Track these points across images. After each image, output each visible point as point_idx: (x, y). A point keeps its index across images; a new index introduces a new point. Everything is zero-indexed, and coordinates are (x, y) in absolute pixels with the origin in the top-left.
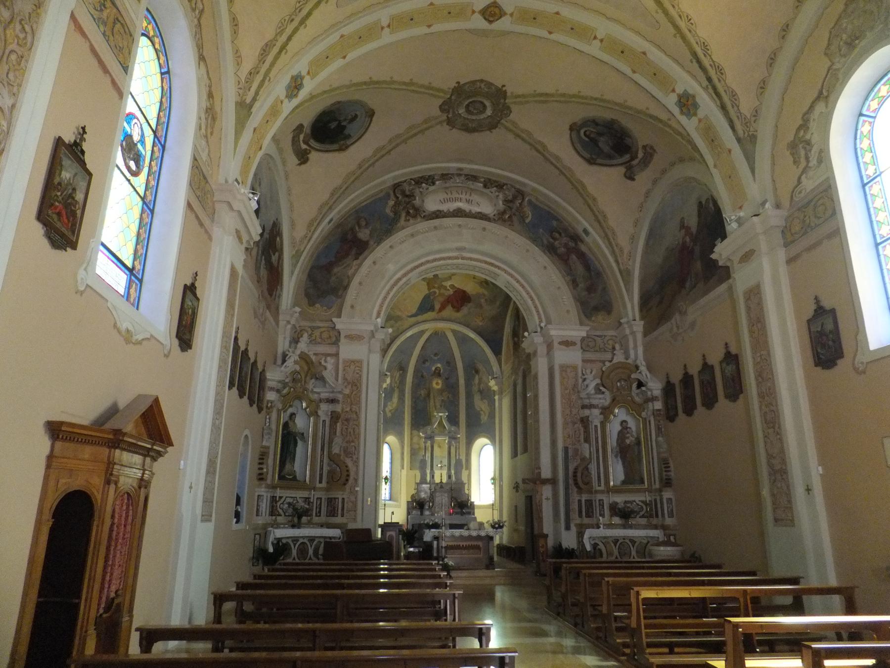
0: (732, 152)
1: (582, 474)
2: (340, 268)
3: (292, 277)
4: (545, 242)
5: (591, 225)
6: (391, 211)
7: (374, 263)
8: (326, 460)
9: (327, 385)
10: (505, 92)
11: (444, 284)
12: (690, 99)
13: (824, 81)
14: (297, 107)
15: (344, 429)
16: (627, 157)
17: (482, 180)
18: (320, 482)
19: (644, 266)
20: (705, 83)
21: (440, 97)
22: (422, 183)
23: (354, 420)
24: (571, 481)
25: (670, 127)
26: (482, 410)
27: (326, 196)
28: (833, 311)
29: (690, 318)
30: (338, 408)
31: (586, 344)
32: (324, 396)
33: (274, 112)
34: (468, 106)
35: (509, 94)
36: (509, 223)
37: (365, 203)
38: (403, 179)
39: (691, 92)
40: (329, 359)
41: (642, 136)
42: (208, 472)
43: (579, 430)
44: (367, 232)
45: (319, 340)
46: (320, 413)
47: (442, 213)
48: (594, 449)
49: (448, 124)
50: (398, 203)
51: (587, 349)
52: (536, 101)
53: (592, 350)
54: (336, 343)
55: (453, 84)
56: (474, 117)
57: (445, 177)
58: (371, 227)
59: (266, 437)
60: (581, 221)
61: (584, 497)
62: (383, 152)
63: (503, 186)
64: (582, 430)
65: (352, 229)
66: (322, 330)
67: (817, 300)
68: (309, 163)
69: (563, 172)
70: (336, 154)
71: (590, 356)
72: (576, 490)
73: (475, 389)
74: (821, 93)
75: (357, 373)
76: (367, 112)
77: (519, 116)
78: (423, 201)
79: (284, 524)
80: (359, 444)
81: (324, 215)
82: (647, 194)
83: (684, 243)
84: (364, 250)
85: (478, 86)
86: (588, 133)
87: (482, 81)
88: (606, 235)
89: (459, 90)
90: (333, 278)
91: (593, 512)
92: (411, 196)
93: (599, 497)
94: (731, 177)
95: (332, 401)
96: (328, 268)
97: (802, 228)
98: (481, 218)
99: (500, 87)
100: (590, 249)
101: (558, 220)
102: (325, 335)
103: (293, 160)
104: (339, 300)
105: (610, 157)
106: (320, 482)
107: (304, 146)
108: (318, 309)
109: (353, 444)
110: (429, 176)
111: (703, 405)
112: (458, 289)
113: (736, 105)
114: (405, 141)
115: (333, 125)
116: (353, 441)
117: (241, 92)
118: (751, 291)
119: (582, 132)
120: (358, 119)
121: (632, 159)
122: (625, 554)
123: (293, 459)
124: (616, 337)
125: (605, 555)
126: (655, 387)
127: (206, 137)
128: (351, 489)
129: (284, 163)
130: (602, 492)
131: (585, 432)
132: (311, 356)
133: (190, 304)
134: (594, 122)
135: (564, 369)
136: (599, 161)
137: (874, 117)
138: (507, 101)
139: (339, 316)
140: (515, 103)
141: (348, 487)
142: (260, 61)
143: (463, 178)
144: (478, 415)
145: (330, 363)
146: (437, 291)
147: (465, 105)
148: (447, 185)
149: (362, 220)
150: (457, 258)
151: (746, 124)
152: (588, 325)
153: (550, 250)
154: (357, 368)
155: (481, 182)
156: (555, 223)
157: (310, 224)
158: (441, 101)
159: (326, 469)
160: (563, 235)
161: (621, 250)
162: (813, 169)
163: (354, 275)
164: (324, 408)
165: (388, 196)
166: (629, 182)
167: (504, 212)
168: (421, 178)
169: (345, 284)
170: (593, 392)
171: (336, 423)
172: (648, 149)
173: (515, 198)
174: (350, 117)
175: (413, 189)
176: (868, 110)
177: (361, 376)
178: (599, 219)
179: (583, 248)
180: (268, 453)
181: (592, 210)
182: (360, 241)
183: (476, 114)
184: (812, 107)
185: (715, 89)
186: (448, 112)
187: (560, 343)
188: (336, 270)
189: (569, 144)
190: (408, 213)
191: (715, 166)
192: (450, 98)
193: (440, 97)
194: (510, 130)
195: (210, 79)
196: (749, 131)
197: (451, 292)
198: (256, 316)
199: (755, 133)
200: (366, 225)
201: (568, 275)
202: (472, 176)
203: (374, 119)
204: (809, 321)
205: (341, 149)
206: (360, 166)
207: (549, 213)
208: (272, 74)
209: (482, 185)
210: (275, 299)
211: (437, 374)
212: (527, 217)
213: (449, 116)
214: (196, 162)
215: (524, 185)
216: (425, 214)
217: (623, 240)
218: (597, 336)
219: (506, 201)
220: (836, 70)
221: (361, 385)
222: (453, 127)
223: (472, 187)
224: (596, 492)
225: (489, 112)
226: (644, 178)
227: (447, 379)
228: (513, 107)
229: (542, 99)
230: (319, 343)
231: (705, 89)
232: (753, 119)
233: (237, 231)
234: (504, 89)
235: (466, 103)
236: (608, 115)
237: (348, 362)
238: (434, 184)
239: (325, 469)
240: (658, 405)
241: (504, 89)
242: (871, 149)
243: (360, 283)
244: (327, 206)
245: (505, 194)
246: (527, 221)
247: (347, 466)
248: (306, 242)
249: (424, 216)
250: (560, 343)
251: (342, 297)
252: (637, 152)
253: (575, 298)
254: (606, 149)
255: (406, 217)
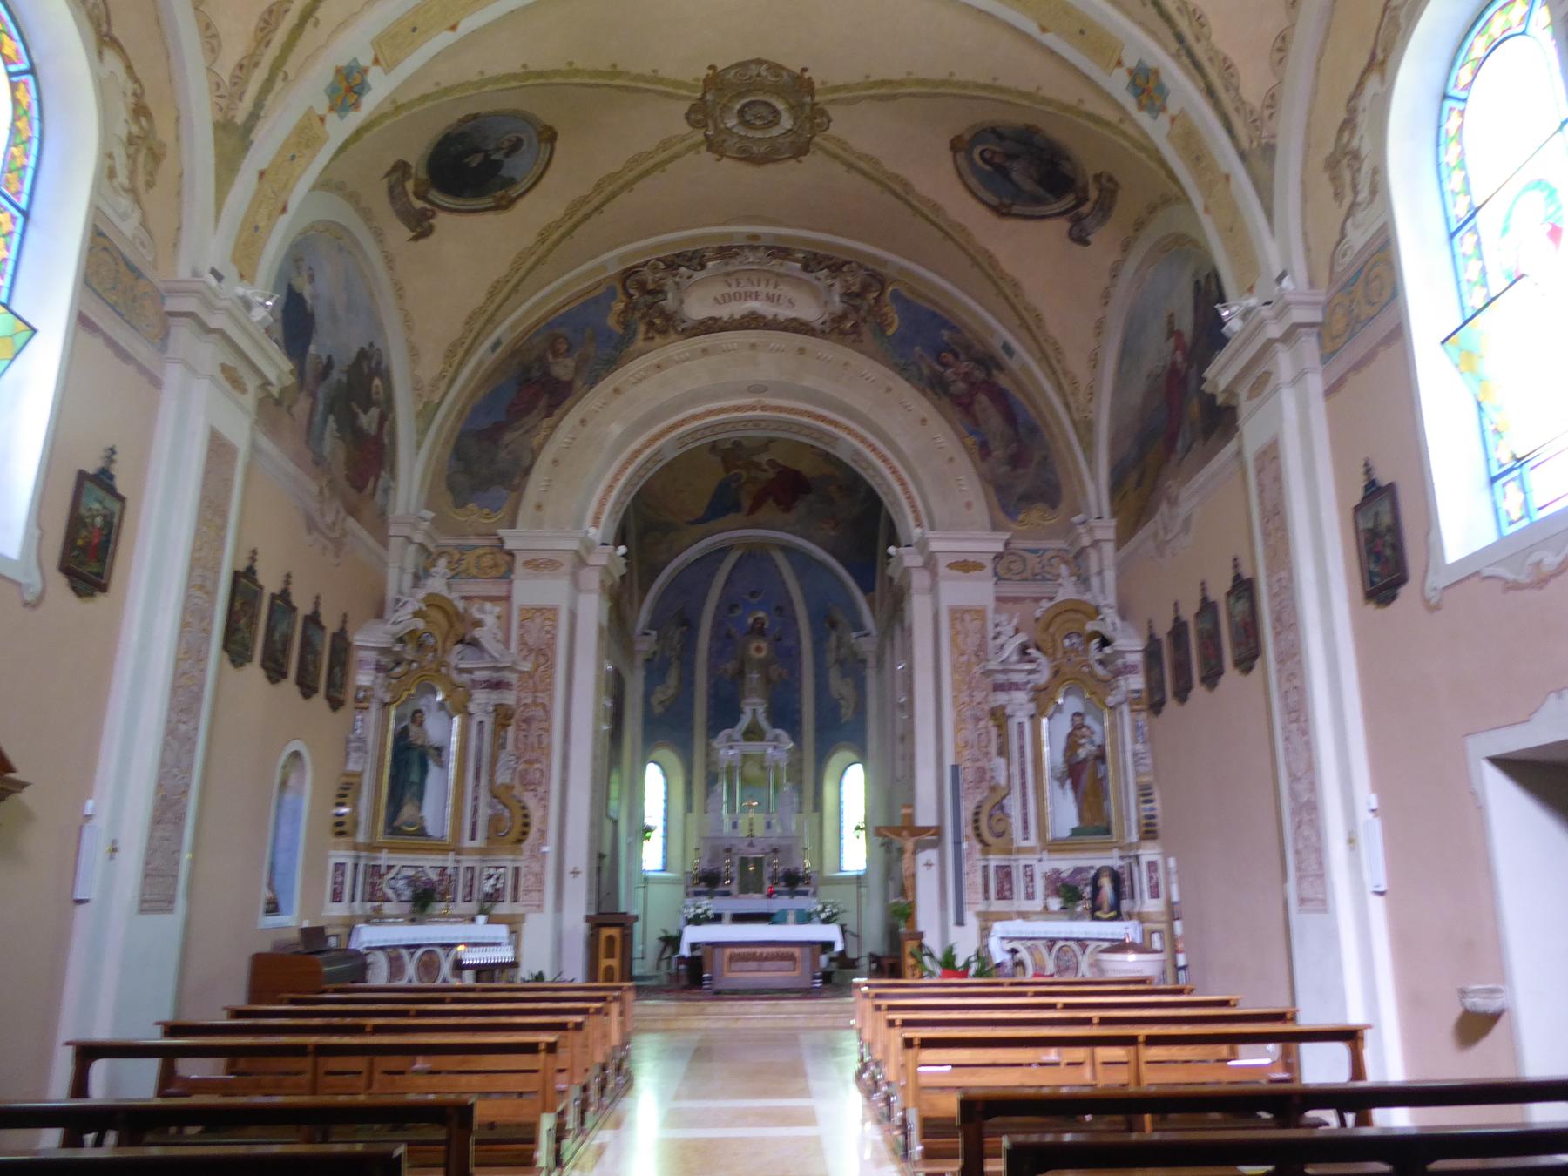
0: (1232, 179)
1: (991, 817)
2: (516, 434)
3: (417, 454)
4: (926, 371)
5: (1016, 336)
6: (618, 322)
7: (583, 422)
8: (484, 797)
9: (486, 656)
10: (810, 82)
11: (756, 458)
12: (1152, 77)
13: (1379, 28)
14: (359, 133)
15: (521, 737)
16: (1069, 200)
17: (800, 256)
18: (473, 838)
19: (1115, 416)
20: (1174, 46)
21: (684, 98)
22: (680, 266)
23: (541, 721)
24: (967, 830)
25: (1124, 134)
26: (843, 698)
27: (479, 298)
28: (1391, 489)
29: (1183, 510)
30: (509, 698)
31: (1004, 565)
32: (480, 675)
33: (306, 137)
34: (741, 112)
35: (817, 85)
36: (853, 337)
37: (566, 309)
38: (643, 260)
39: (1150, 64)
40: (488, 606)
41: (1089, 162)
42: (157, 820)
43: (988, 732)
44: (570, 363)
45: (474, 571)
46: (472, 708)
47: (720, 323)
48: (1015, 769)
49: (709, 149)
50: (630, 308)
51: (1006, 576)
52: (872, 97)
53: (1017, 577)
54: (507, 575)
55: (703, 72)
56: (759, 134)
57: (726, 252)
58: (576, 355)
59: (353, 755)
60: (999, 332)
61: (994, 861)
62: (585, 210)
63: (843, 265)
64: (994, 732)
65: (541, 359)
66: (481, 551)
67: (1368, 470)
68: (433, 237)
69: (951, 234)
70: (490, 216)
71: (1010, 589)
72: (979, 846)
73: (831, 657)
74: (1373, 56)
75: (548, 632)
76: (539, 134)
77: (844, 125)
78: (682, 302)
79: (397, 917)
80: (549, 766)
81: (479, 334)
82: (1115, 273)
83: (1174, 363)
84: (565, 398)
85: (755, 73)
86: (987, 155)
87: (759, 62)
88: (1043, 351)
89: (715, 81)
90: (502, 454)
91: (1011, 889)
92: (659, 292)
93: (1024, 860)
94: (1235, 231)
95: (496, 685)
96: (492, 435)
97: (1348, 325)
98: (796, 331)
99: (799, 72)
100: (1017, 383)
101: (952, 328)
102: (487, 561)
103: (400, 233)
104: (514, 494)
105: (1038, 201)
106: (473, 838)
107: (419, 204)
108: (473, 514)
109: (536, 766)
110: (694, 252)
111: (1204, 680)
112: (785, 467)
113: (1232, 87)
114: (628, 186)
115: (475, 161)
116: (537, 761)
117: (223, 102)
118: (1265, 453)
119: (977, 152)
120: (524, 148)
121: (1082, 201)
122: (1067, 968)
123: (420, 796)
124: (1066, 550)
125: (1030, 971)
126: (1130, 645)
127: (132, 191)
128: (532, 851)
129: (379, 236)
130: (1031, 850)
131: (999, 736)
132: (456, 602)
133: (96, 506)
134: (995, 133)
135: (958, 615)
136: (1016, 209)
137: (1465, 100)
138: (817, 99)
139: (512, 525)
140: (833, 102)
141: (526, 846)
142: (259, 43)
143: (761, 254)
144: (836, 708)
145: (489, 615)
146: (744, 474)
147: (735, 111)
148: (730, 268)
149: (561, 340)
150: (753, 408)
151: (1255, 123)
152: (1008, 530)
153: (935, 386)
154: (548, 622)
155: (797, 261)
156: (946, 335)
157: (450, 353)
158: (685, 107)
159: (484, 812)
160: (962, 357)
161: (1074, 383)
162: (1363, 207)
163: (542, 446)
164: (482, 701)
165: (611, 294)
166: (1077, 248)
167: (843, 317)
168: (678, 256)
169: (526, 463)
170: (1015, 658)
171: (505, 726)
172: (1104, 181)
173: (865, 288)
174: (506, 144)
175: (661, 279)
176: (1456, 86)
177: (553, 638)
178: (1029, 324)
179: (1003, 381)
180: (359, 786)
181: (1013, 307)
182: (558, 381)
183: (762, 127)
184: (1361, 84)
185: (1191, 54)
186: (706, 126)
187: (951, 566)
188: (508, 437)
189: (954, 177)
190: (651, 325)
191: (1207, 210)
192: (702, 99)
193: (684, 98)
194: (836, 157)
195: (136, 81)
196: (1260, 137)
197: (772, 474)
198: (311, 526)
199: (1272, 141)
200: (568, 350)
201: (971, 434)
202: (780, 249)
203: (558, 144)
204: (1357, 509)
205: (503, 205)
206: (542, 238)
207: (934, 315)
208: (290, 67)
209: (799, 265)
210: (373, 494)
211: (758, 630)
212: (890, 325)
213: (708, 133)
214: (100, 239)
215: (884, 263)
216: (683, 326)
217: (1076, 363)
218: (1030, 551)
219: (847, 295)
220: (1395, 8)
221: (554, 653)
222: (722, 155)
223: (782, 270)
224: (1021, 850)
225: (786, 122)
226: (1103, 239)
227: (779, 639)
228: (833, 111)
229: (883, 91)
230: (475, 577)
231: (1176, 57)
232: (1267, 112)
233: (224, 369)
234: (806, 75)
235: (738, 106)
236: (1018, 119)
237: (528, 610)
238: (703, 267)
239: (481, 812)
240: (1137, 682)
241: (806, 75)
242: (1462, 166)
243: (555, 462)
244: (483, 319)
245: (847, 281)
246: (890, 332)
247: (524, 808)
248: (443, 385)
249: (683, 330)
250: (951, 566)
251: (519, 489)
252: (1085, 189)
253: (981, 476)
254: (1028, 185)
255: (647, 332)
